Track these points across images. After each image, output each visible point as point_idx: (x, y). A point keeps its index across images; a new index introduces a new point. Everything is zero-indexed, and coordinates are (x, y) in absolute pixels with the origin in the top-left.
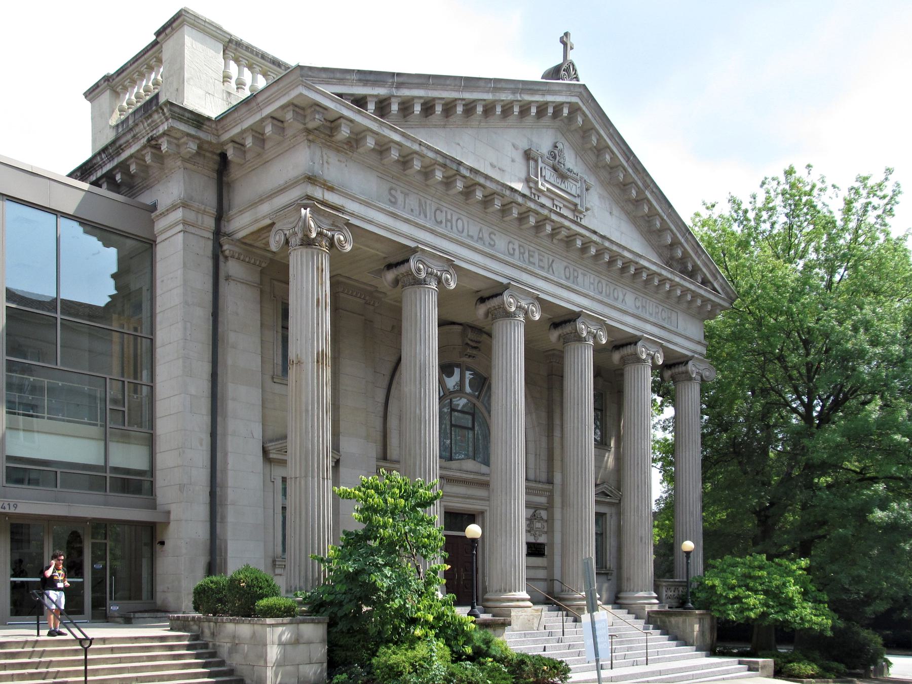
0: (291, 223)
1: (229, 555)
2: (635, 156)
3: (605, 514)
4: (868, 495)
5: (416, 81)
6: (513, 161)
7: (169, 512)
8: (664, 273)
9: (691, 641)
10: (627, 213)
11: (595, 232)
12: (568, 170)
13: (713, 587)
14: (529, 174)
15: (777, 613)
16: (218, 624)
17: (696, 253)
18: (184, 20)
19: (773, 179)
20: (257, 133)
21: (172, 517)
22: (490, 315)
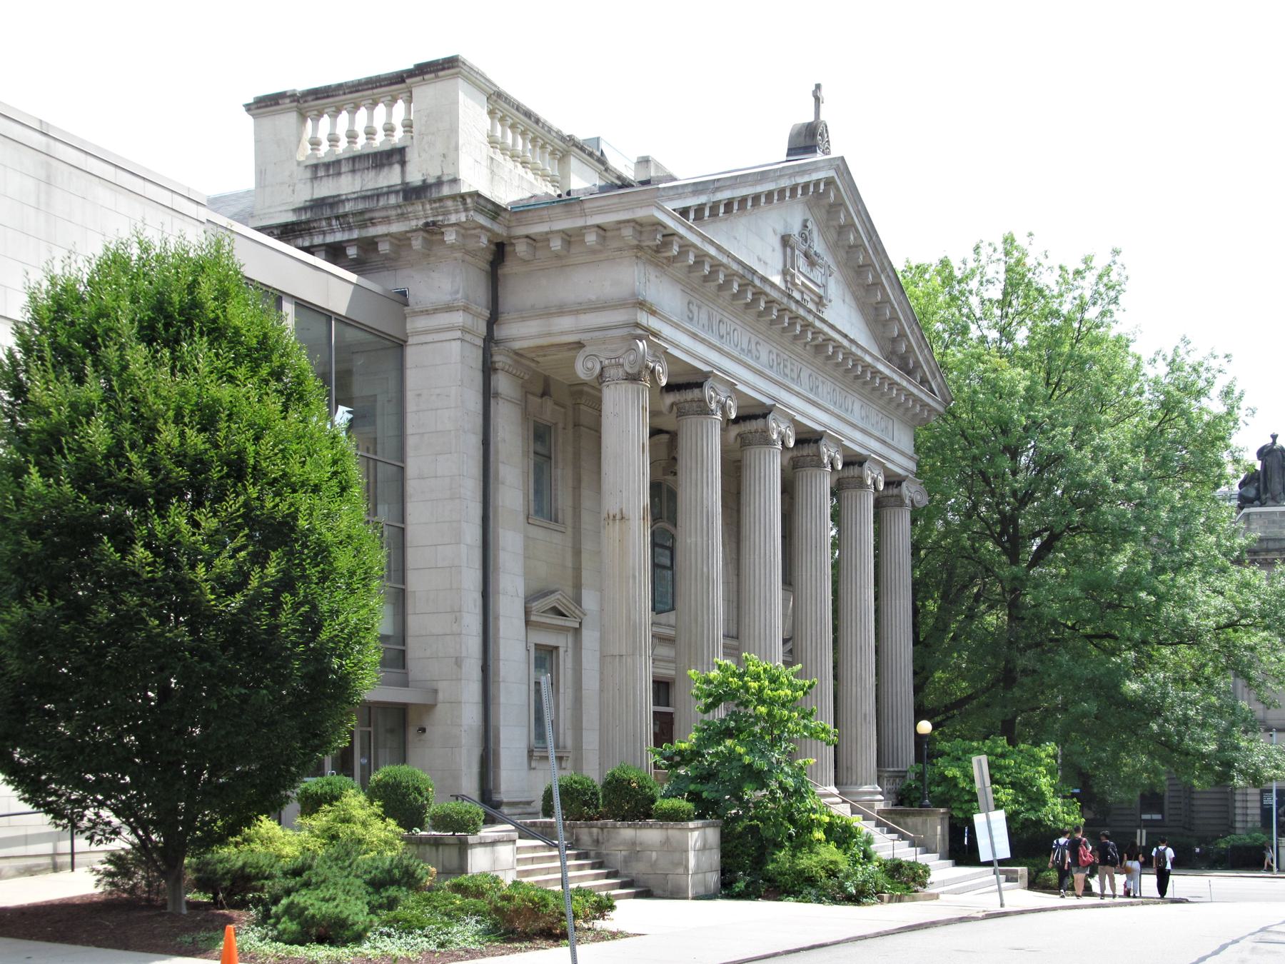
0: (612, 351)
1: (502, 745)
2: (877, 236)
3: (557, 648)
4: (1115, 663)
5: (728, 183)
6: (773, 250)
7: (436, 691)
8: (881, 367)
9: (934, 847)
10: (856, 299)
11: (846, 336)
12: (816, 254)
13: (954, 778)
14: (785, 265)
15: (1027, 810)
16: (605, 830)
17: (920, 347)
18: (459, 73)
19: (990, 244)
20: (570, 238)
21: (441, 696)
22: (675, 408)
